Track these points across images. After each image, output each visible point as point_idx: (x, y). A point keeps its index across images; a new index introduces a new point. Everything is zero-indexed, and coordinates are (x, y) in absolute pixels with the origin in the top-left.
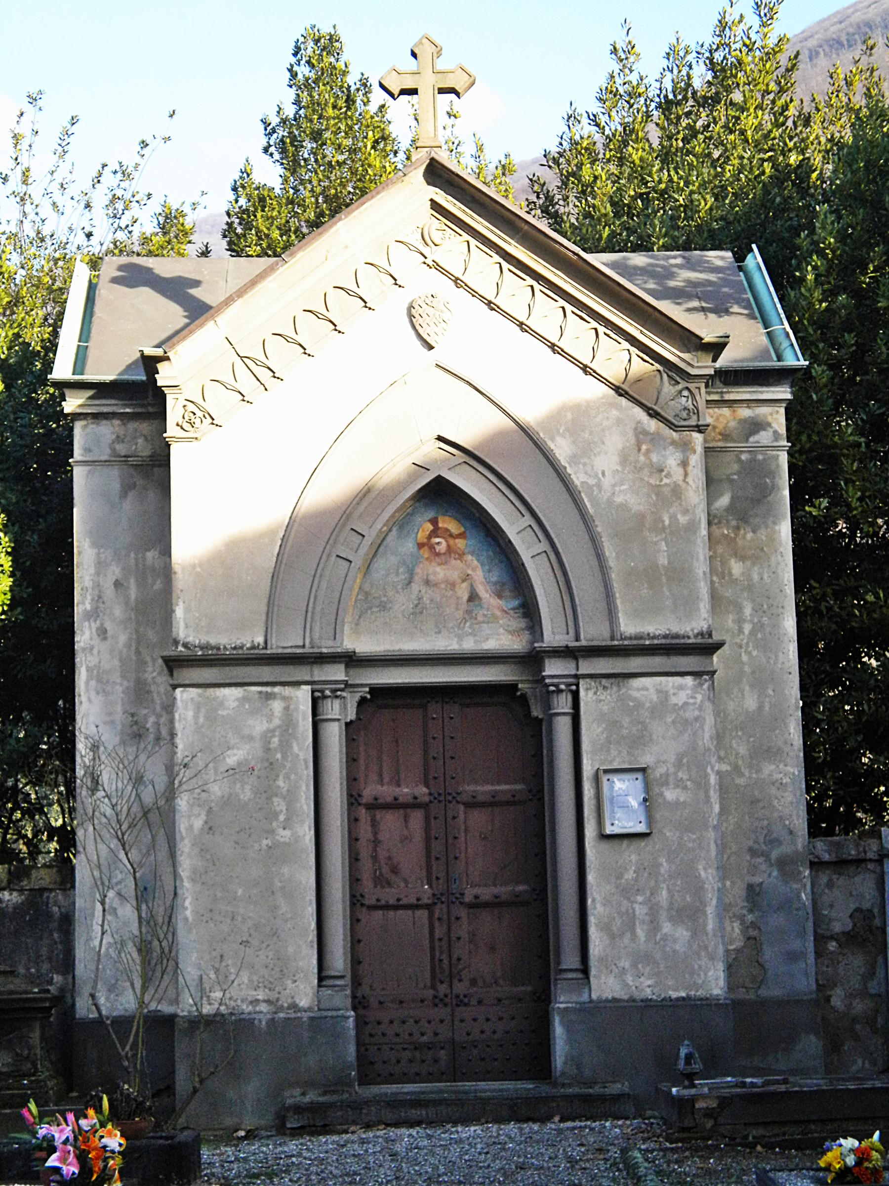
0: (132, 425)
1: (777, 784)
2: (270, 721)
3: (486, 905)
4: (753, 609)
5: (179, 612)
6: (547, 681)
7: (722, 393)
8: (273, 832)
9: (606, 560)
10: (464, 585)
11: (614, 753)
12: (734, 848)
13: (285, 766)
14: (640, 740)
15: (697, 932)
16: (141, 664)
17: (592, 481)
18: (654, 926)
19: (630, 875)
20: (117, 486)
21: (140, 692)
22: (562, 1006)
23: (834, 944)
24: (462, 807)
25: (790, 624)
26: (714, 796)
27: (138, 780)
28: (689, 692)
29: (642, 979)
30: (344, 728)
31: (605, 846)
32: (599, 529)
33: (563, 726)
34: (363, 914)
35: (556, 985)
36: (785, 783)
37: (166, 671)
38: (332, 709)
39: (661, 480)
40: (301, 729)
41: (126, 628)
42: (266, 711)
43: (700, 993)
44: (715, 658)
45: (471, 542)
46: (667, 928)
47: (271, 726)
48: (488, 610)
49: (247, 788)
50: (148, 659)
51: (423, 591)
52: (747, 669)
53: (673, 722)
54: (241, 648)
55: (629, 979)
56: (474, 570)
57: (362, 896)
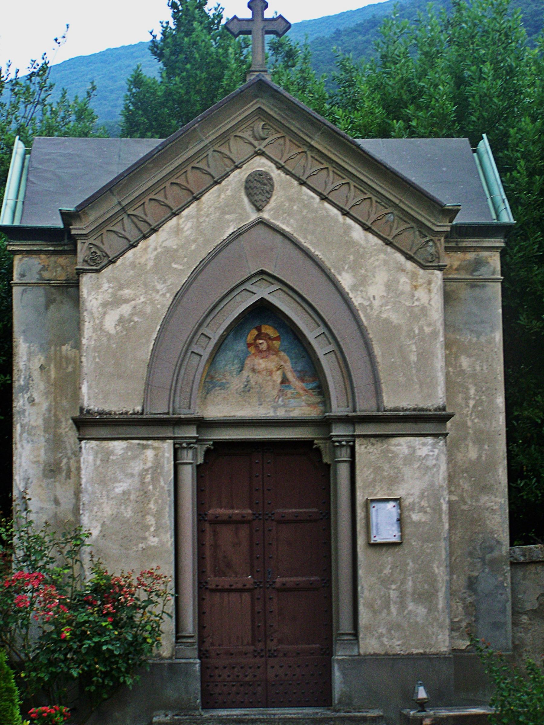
0: (53, 258)
1: (489, 510)
2: (145, 464)
3: (290, 590)
4: (476, 390)
5: (84, 389)
6: (334, 439)
7: (457, 242)
8: (145, 539)
9: (375, 357)
10: (279, 372)
11: (378, 488)
12: (459, 553)
13: (154, 495)
14: (394, 480)
16: (58, 421)
17: (366, 303)
18: (402, 605)
19: (387, 571)
20: (42, 300)
21: (55, 443)
22: (340, 658)
23: (526, 617)
24: (274, 523)
25: (500, 401)
26: (445, 518)
27: (57, 502)
28: (429, 447)
29: (394, 640)
30: (195, 468)
31: (370, 551)
32: (371, 336)
33: (343, 470)
34: (207, 596)
35: (336, 643)
36: (495, 508)
37: (74, 428)
38: (187, 456)
39: (413, 303)
40: (166, 469)
41: (47, 398)
42: (142, 457)
43: (433, 650)
44: (449, 424)
45: (285, 343)
46: (411, 606)
47: (146, 467)
48: (295, 389)
49: (129, 509)
50: (63, 419)
51: (251, 376)
52: (471, 431)
53: (418, 468)
54: (126, 413)
55: (385, 640)
56: (285, 362)
57: (207, 583)
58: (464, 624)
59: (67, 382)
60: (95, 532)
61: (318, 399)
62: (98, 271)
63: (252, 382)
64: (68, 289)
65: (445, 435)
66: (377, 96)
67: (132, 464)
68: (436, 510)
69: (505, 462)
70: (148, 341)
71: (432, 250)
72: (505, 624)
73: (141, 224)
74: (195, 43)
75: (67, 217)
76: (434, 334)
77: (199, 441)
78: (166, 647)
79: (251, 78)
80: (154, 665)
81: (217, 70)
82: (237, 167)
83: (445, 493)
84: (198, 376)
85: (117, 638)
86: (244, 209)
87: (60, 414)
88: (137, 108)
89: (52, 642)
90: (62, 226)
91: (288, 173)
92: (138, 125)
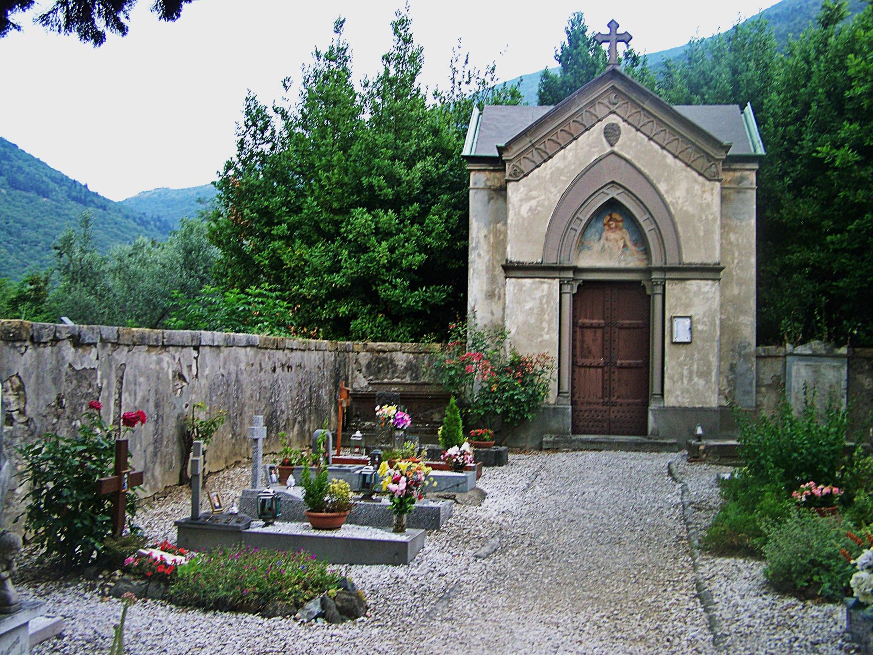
0: (493, 174)
5: (509, 249)
8: (542, 336)
14: (688, 306)
15: (707, 382)
16: (494, 267)
17: (674, 201)
18: (690, 379)
19: (682, 358)
20: (486, 198)
21: (493, 280)
27: (492, 313)
31: (673, 346)
44: (722, 273)
46: (696, 379)
58: (727, 391)
59: (499, 244)
60: (513, 331)
61: (645, 257)
62: (518, 181)
63: (606, 246)
64: (500, 191)
65: (719, 280)
66: (685, 81)
67: (535, 292)
68: (713, 324)
69: (755, 297)
70: (546, 222)
71: (715, 170)
72: (751, 392)
73: (543, 154)
74: (579, 53)
75: (500, 150)
76: (715, 219)
77: (574, 280)
78: (552, 398)
79: (609, 68)
80: (544, 409)
81: (592, 69)
82: (599, 121)
83: (718, 314)
84: (574, 242)
85: (524, 392)
86: (603, 145)
87: (495, 263)
88: (545, 91)
89: (486, 393)
90: (497, 155)
91: (629, 124)
92: (546, 100)
